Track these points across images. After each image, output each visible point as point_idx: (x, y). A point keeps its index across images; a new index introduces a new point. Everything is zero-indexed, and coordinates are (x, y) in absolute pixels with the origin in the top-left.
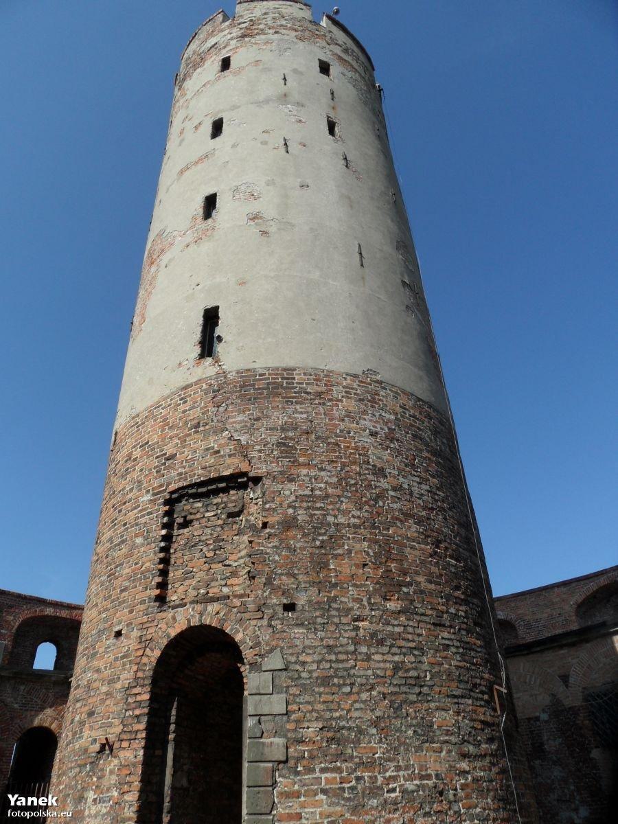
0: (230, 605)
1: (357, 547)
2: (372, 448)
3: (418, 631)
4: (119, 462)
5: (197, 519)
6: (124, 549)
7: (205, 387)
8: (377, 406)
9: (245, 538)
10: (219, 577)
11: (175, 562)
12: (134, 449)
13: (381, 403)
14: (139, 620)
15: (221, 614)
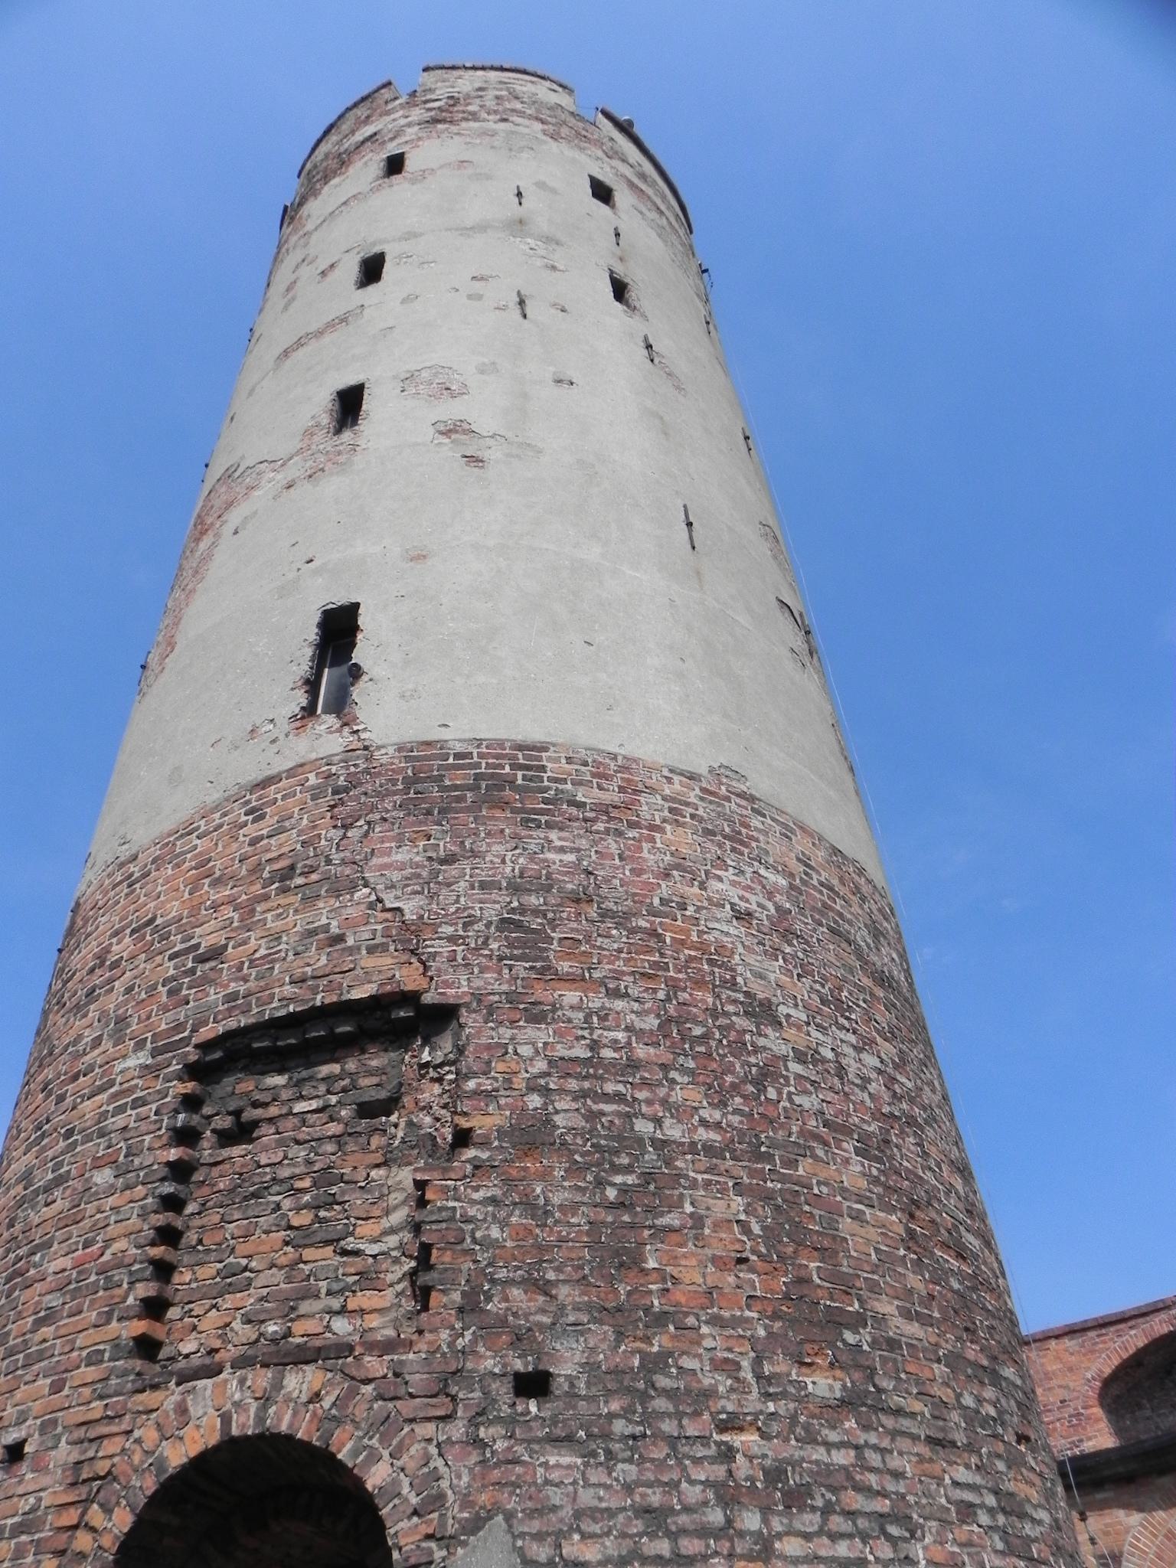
0: (354, 1373)
1: (719, 1208)
2: (741, 950)
3: (895, 1462)
4: (74, 974)
5: (270, 1120)
6: (59, 1201)
7: (313, 780)
8: (746, 851)
9: (405, 1176)
10: (323, 1285)
11: (200, 1242)
12: (114, 940)
13: (754, 844)
14: (78, 1414)
15: (327, 1403)
